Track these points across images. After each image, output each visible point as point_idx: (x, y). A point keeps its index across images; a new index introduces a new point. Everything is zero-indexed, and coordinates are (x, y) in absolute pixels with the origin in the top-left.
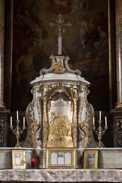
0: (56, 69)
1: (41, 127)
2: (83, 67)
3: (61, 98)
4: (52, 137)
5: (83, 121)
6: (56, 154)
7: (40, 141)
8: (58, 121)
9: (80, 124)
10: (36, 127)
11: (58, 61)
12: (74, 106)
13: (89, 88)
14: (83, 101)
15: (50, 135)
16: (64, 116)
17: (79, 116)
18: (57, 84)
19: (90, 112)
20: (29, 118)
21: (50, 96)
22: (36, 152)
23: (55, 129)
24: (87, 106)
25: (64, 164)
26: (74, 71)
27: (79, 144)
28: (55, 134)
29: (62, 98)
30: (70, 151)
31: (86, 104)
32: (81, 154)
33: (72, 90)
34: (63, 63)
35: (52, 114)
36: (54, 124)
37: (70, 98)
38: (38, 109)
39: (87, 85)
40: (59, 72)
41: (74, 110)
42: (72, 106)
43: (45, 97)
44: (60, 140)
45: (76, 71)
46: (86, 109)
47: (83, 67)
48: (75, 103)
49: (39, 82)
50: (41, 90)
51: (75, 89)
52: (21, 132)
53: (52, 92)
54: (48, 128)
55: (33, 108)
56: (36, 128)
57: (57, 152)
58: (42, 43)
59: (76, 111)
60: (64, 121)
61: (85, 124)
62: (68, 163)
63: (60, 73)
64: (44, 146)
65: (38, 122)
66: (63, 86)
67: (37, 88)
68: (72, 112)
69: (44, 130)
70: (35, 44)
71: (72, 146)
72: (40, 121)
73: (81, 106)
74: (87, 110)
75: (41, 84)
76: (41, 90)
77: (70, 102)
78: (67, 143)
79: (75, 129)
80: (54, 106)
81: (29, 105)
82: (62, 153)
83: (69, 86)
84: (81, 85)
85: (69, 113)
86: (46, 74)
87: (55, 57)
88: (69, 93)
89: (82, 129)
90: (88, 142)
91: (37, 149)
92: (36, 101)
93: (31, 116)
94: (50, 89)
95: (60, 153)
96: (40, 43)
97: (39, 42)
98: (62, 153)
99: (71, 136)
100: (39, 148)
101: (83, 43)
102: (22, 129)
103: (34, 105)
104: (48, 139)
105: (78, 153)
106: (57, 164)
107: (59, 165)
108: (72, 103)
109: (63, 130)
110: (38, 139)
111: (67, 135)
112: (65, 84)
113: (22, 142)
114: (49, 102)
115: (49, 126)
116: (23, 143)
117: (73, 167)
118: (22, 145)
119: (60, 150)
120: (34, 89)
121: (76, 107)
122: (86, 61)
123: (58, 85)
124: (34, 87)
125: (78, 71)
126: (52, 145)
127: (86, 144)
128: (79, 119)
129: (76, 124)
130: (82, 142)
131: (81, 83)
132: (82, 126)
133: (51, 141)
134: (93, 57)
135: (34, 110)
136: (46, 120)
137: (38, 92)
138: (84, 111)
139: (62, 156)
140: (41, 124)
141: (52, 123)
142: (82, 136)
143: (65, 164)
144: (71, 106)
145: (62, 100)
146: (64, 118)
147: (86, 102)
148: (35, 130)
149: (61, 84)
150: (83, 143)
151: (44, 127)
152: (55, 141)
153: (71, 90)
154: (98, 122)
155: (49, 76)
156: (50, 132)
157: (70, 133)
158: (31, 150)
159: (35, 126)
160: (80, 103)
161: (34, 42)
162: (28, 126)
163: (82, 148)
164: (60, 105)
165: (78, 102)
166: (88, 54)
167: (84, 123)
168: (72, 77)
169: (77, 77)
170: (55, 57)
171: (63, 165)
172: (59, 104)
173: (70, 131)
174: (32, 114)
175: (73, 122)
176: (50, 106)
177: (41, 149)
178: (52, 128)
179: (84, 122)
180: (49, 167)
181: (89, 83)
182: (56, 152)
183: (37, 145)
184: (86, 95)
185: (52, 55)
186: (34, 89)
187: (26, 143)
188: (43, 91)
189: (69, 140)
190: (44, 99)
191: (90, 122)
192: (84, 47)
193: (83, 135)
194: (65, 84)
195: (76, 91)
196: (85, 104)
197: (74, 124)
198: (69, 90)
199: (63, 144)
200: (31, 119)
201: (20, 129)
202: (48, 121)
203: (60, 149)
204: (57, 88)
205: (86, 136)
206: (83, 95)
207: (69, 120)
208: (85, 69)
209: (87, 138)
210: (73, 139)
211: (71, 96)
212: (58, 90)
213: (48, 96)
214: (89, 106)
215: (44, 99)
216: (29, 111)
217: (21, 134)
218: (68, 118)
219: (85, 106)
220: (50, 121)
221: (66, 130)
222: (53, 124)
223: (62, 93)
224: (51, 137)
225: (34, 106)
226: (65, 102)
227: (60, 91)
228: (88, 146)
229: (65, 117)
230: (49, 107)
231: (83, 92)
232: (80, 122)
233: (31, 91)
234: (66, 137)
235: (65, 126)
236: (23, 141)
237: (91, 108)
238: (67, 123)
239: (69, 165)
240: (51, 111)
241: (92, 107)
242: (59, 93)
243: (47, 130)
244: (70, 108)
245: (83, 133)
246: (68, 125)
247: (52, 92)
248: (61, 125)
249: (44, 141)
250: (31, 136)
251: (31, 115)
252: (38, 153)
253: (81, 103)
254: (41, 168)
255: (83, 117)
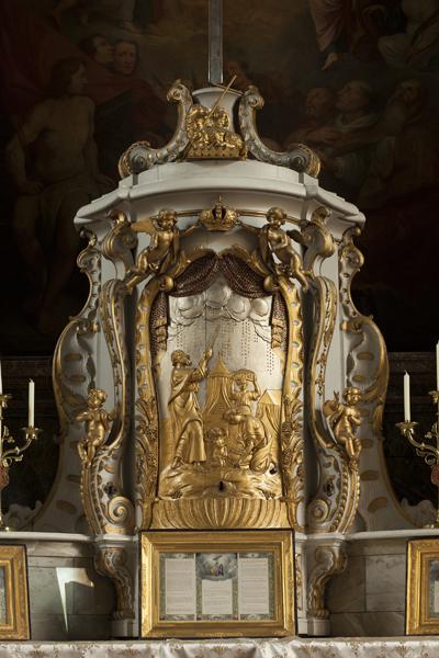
0: (198, 138)
1: (125, 426)
2: (330, 150)
3: (222, 285)
4: (178, 479)
5: (336, 395)
6: (193, 561)
7: (118, 499)
8: (207, 397)
9: (318, 412)
10: (101, 427)
11: (212, 107)
12: (288, 327)
13: (359, 242)
14: (330, 296)
15: (169, 468)
16: (236, 373)
17: (316, 370)
18: (200, 211)
19: (369, 356)
20: (71, 387)
21: (166, 273)
22: (100, 552)
23: (190, 434)
24: (355, 329)
25: (235, 612)
26: (285, 158)
27: (318, 513)
28: (191, 459)
29: (223, 280)
30: (266, 544)
31: (346, 318)
32: (327, 561)
33: (279, 241)
34: (230, 120)
35: (175, 365)
36: (188, 413)
37: (267, 281)
38: (110, 339)
39: (351, 229)
40: (213, 153)
41: (287, 339)
42: (274, 321)
43: (142, 276)
44: (216, 491)
45: (295, 155)
46: (347, 343)
47: (330, 150)
48: (294, 309)
49: (115, 208)
50: (125, 247)
51: (291, 234)
52: (14, 455)
53: (179, 251)
54: (159, 434)
55: (89, 341)
56: (96, 435)
57: (198, 555)
58: (132, 42)
59: (296, 349)
60: (239, 395)
61: (344, 413)
62: (255, 605)
63: (217, 158)
64: (139, 525)
65: (109, 407)
66: (233, 223)
67: (104, 240)
68: (278, 354)
69: (138, 446)
70: (103, 52)
71: (279, 520)
72: (122, 398)
73: (325, 322)
74: (351, 350)
75: (122, 219)
76: (125, 247)
77: (266, 303)
78: (257, 507)
79: (294, 439)
80: (188, 321)
81: (67, 328)
82: (222, 561)
83: (261, 222)
84: (323, 223)
85: (262, 357)
86: (146, 169)
87: (194, 93)
88: (264, 257)
89: (327, 438)
90: (359, 502)
91: (105, 537)
92: (102, 302)
93: (78, 379)
94: (166, 236)
95: (210, 559)
96: (124, 46)
97: (120, 41)
98: (222, 561)
99: (272, 472)
100: (114, 534)
101: (325, 41)
102: (20, 441)
103: (95, 327)
104: (157, 485)
105: (314, 555)
106: (199, 612)
107: (207, 617)
108: (277, 305)
109: (231, 442)
110: (110, 491)
111: (252, 466)
112: (243, 213)
113: (33, 508)
114: (161, 305)
115: (161, 421)
116: (35, 511)
117: (282, 627)
118: (32, 523)
119: (215, 538)
120: (92, 252)
121: (296, 327)
122: (344, 120)
123: (207, 214)
124: (91, 242)
125: (303, 152)
126: (177, 518)
127: (353, 512)
128: (315, 388)
129: (301, 414)
130: (333, 499)
131: (322, 208)
132: (328, 421)
133: (172, 495)
134: (374, 103)
135: (95, 348)
136: (149, 393)
137: (111, 256)
138: (336, 349)
139: (220, 573)
140: (127, 416)
141: (178, 408)
142: (331, 471)
143: (241, 612)
144: (270, 324)
145: (228, 292)
146: (239, 383)
147: (346, 311)
148: (96, 442)
149: (224, 212)
150: (334, 505)
151: (139, 428)
152: (193, 498)
153: (270, 240)
154: (399, 430)
155: (162, 176)
156: (165, 454)
157: (268, 452)
158: (76, 543)
159: (92, 423)
160: (319, 309)
161: (97, 41)
162: (63, 426)
163: (331, 530)
164: (217, 318)
165: (310, 299)
166: (353, 92)
167: (341, 408)
168: (277, 177)
169: (301, 181)
170: (194, 93)
171: (228, 617)
172: (210, 314)
173: (267, 447)
174: (85, 370)
175: (285, 402)
176: (168, 324)
177: (126, 539)
178: (178, 433)
179: (341, 400)
180: (155, 629)
181: (361, 217)
182: (189, 555)
183: (105, 521)
184: (347, 275)
185: (178, 81)
186: (92, 252)
187: (52, 506)
188: (134, 251)
189: (265, 493)
190: (141, 287)
191: (366, 407)
192: (332, 58)
193: (337, 469)
194: (243, 213)
195: (296, 247)
196: (340, 316)
197: (290, 411)
198: (262, 240)
199: (232, 512)
200: (78, 396)
201: (11, 440)
202: (157, 397)
203: (210, 538)
204: (201, 230)
205: (351, 473)
206: (333, 272)
207: (261, 389)
208: (341, 162)
209: (354, 484)
210: (286, 484)
211: (272, 272)
212: (207, 243)
213: (159, 275)
214: (360, 326)
215: (141, 287)
216: (69, 358)
217: (13, 465)
218: (258, 382)
219: (345, 326)
220: (166, 396)
221: (247, 442)
222: (182, 414)
223: (227, 256)
224: (174, 477)
225: (91, 332)
226: (243, 304)
227: (218, 247)
228: (361, 525)
229: (243, 376)
230: (162, 330)
231: (330, 254)
232: (317, 403)
233: (80, 262)
234: (249, 477)
235: (242, 422)
236: (38, 503)
237: (372, 337)
238: (252, 408)
239: (258, 620)
240: (173, 345)
241: (378, 331)
242: (211, 255)
243: (152, 441)
244: (266, 332)
245: (337, 455)
246: (259, 417)
247: (179, 251)
248: (225, 416)
249: (139, 496)
250: (75, 479)
251: (77, 376)
252: (110, 557)
253: (326, 305)
254: (126, 635)
255: (333, 377)
